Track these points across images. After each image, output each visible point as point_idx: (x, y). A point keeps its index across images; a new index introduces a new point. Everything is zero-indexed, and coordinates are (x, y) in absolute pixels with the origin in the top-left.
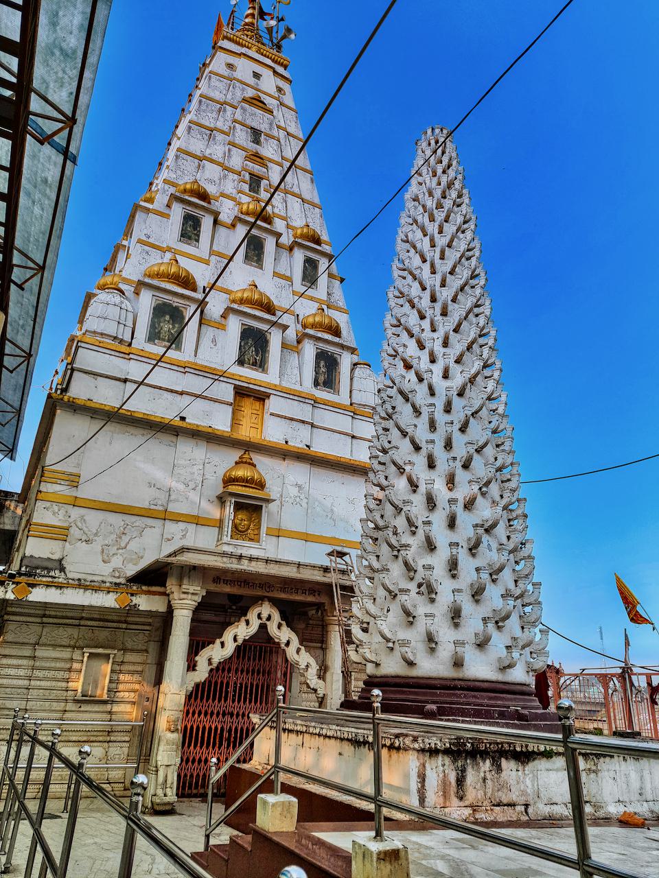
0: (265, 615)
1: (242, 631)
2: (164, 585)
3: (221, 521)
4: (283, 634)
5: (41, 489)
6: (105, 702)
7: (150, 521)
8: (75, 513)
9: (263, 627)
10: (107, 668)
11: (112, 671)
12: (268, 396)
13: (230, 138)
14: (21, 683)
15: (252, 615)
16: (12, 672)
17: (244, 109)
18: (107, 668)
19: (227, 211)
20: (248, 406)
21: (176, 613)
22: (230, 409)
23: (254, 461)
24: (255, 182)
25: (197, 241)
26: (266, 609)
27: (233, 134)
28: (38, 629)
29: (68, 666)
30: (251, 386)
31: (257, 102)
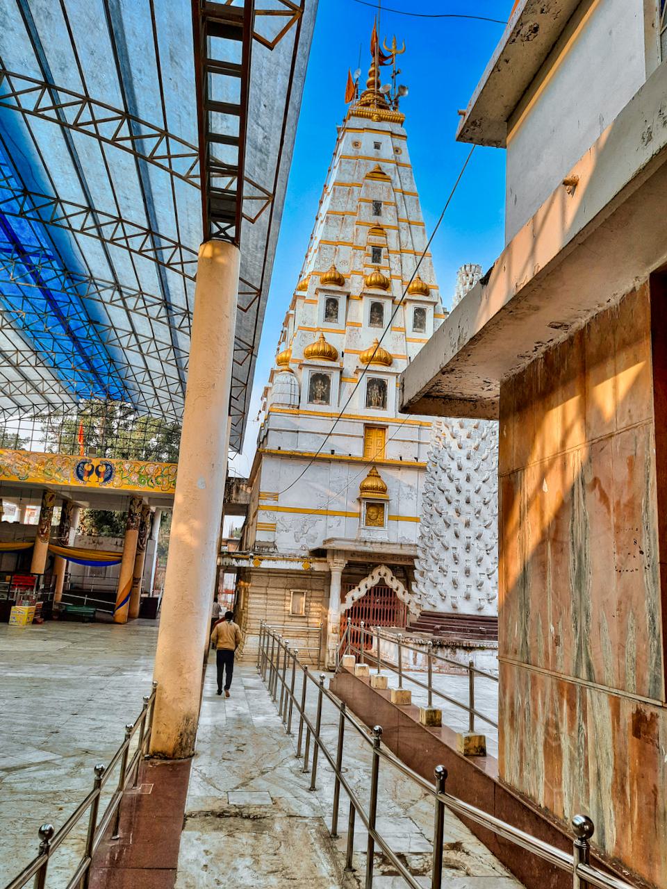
0: (382, 573)
1: (370, 582)
2: (325, 557)
3: (360, 513)
4: (395, 584)
5: (260, 504)
6: (304, 617)
7: (318, 517)
8: (279, 515)
9: (382, 580)
10: (303, 599)
11: (306, 601)
12: (387, 426)
13: (356, 218)
14: (262, 606)
15: (375, 573)
16: (258, 601)
17: (367, 185)
18: (303, 599)
19: (357, 285)
20: (375, 436)
21: (333, 573)
22: (362, 440)
23: (379, 474)
24: (376, 254)
25: (337, 318)
26: (383, 570)
27: (360, 214)
28: (266, 579)
29: (283, 598)
30: (375, 422)
31: (379, 174)
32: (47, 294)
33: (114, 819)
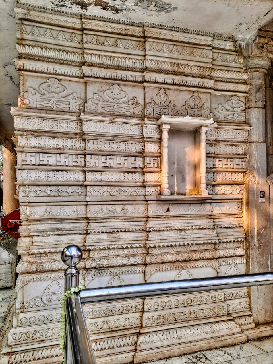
6: (202, 202)
29: (137, 148)
32: (196, 341)
33: (76, 353)
